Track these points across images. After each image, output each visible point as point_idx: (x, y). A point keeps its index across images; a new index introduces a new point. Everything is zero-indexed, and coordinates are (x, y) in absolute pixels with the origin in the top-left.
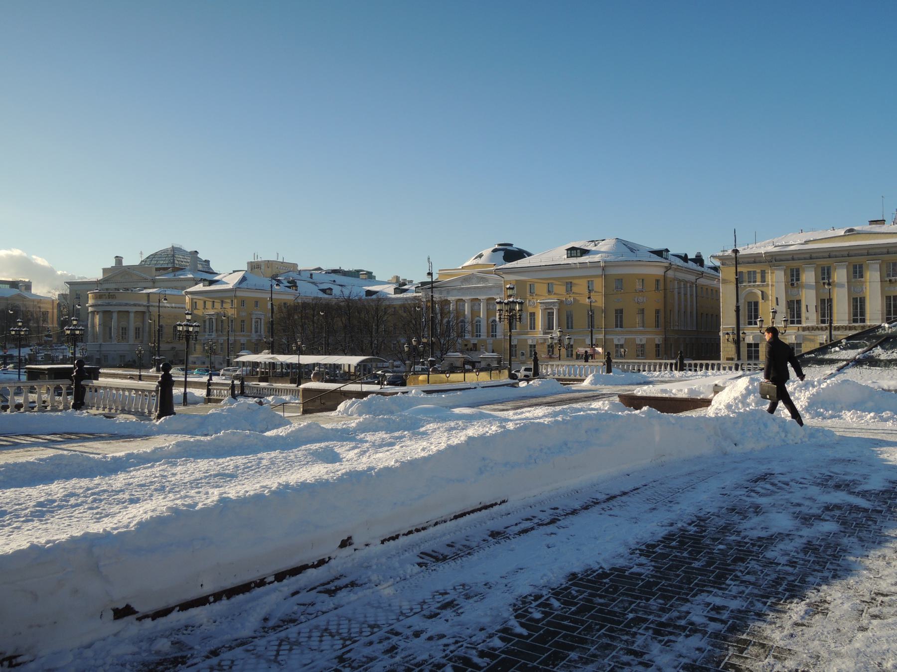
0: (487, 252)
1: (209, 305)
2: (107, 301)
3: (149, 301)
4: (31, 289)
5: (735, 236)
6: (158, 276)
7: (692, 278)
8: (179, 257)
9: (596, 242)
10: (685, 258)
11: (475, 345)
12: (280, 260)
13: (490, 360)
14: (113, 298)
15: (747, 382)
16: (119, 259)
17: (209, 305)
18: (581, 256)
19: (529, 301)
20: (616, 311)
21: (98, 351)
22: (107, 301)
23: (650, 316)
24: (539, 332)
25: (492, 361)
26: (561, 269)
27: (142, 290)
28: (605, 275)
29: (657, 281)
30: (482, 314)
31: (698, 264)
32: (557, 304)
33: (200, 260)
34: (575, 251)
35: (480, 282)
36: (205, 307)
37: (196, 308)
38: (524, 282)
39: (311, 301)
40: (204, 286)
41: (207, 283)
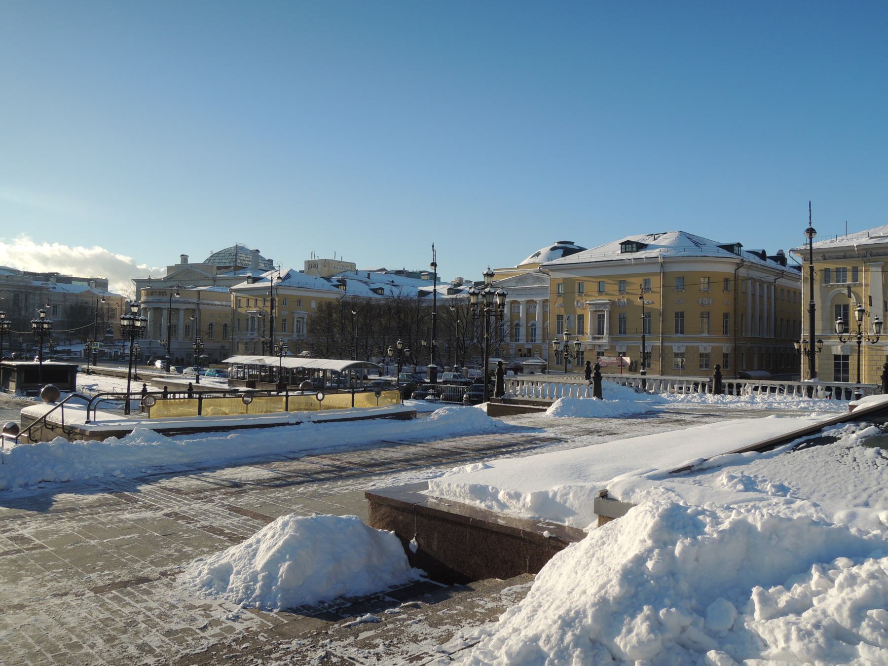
0: (545, 250)
1: (252, 303)
2: (158, 298)
3: (199, 298)
4: (107, 287)
5: (810, 210)
6: (219, 275)
7: (771, 279)
8: (242, 256)
9: (656, 236)
10: (763, 255)
11: (529, 350)
12: (338, 259)
13: (533, 367)
14: (163, 295)
15: (644, 534)
16: (184, 258)
17: (252, 303)
18: (637, 251)
19: (578, 302)
20: (677, 314)
21: (148, 348)
22: (158, 298)
23: (717, 320)
24: (587, 339)
25: (535, 368)
26: (604, 267)
27: (195, 288)
28: (663, 273)
29: (727, 280)
30: (538, 317)
31: (779, 262)
32: (608, 306)
33: (263, 259)
34: (630, 246)
35: (535, 282)
36: (248, 306)
37: (240, 307)
38: (572, 281)
39: (351, 300)
40: (248, 283)
41: (251, 280)
